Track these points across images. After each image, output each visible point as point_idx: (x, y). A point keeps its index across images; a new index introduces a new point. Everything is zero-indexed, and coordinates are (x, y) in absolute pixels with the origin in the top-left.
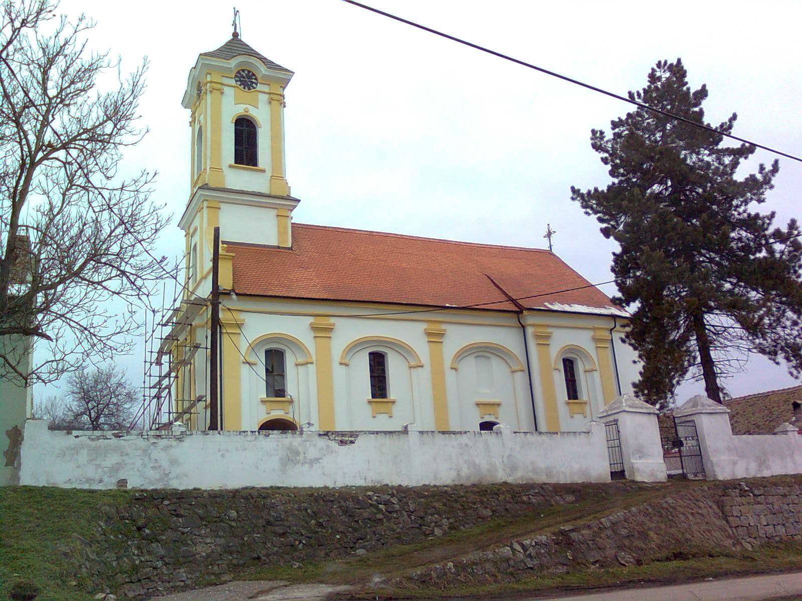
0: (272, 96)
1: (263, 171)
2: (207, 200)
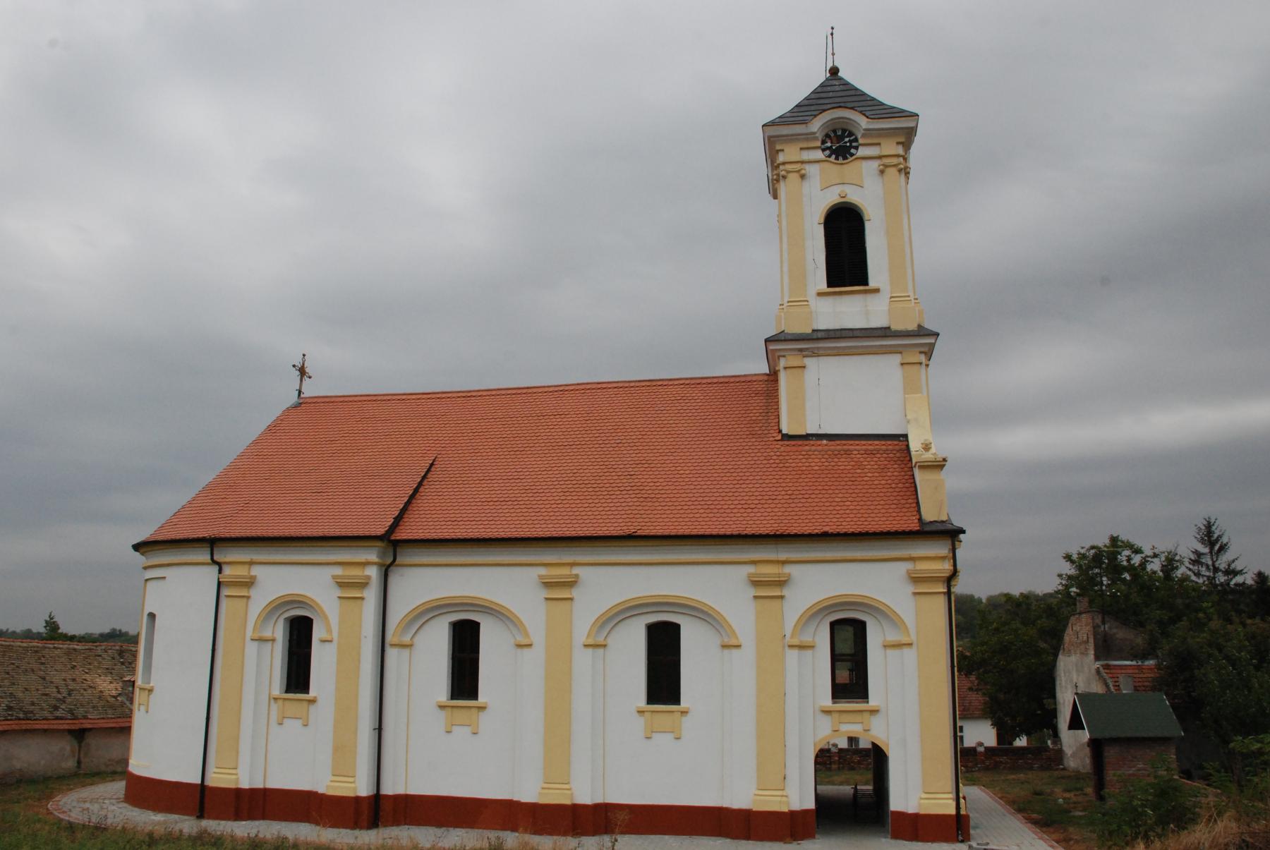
0: (887, 161)
1: (877, 291)
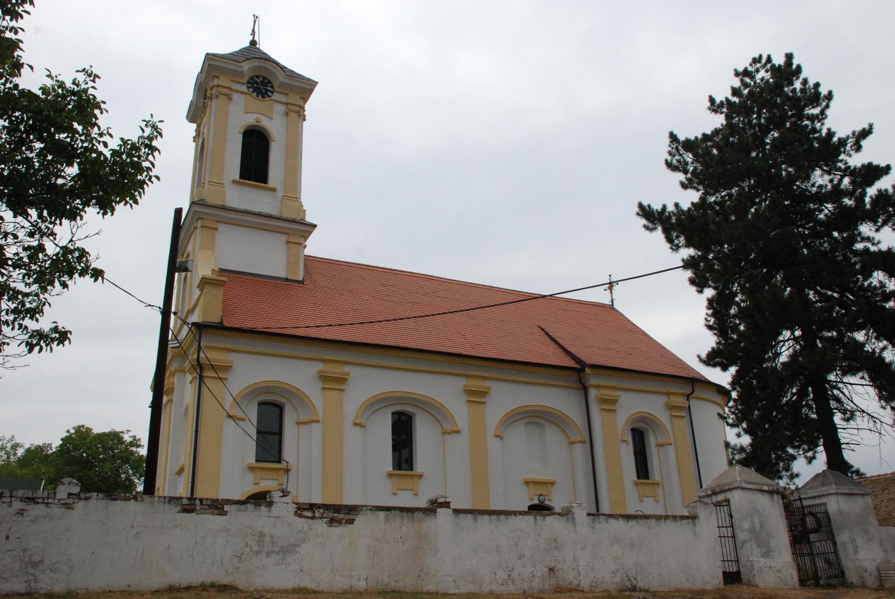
0: (290, 107)
1: (273, 190)
2: (202, 219)
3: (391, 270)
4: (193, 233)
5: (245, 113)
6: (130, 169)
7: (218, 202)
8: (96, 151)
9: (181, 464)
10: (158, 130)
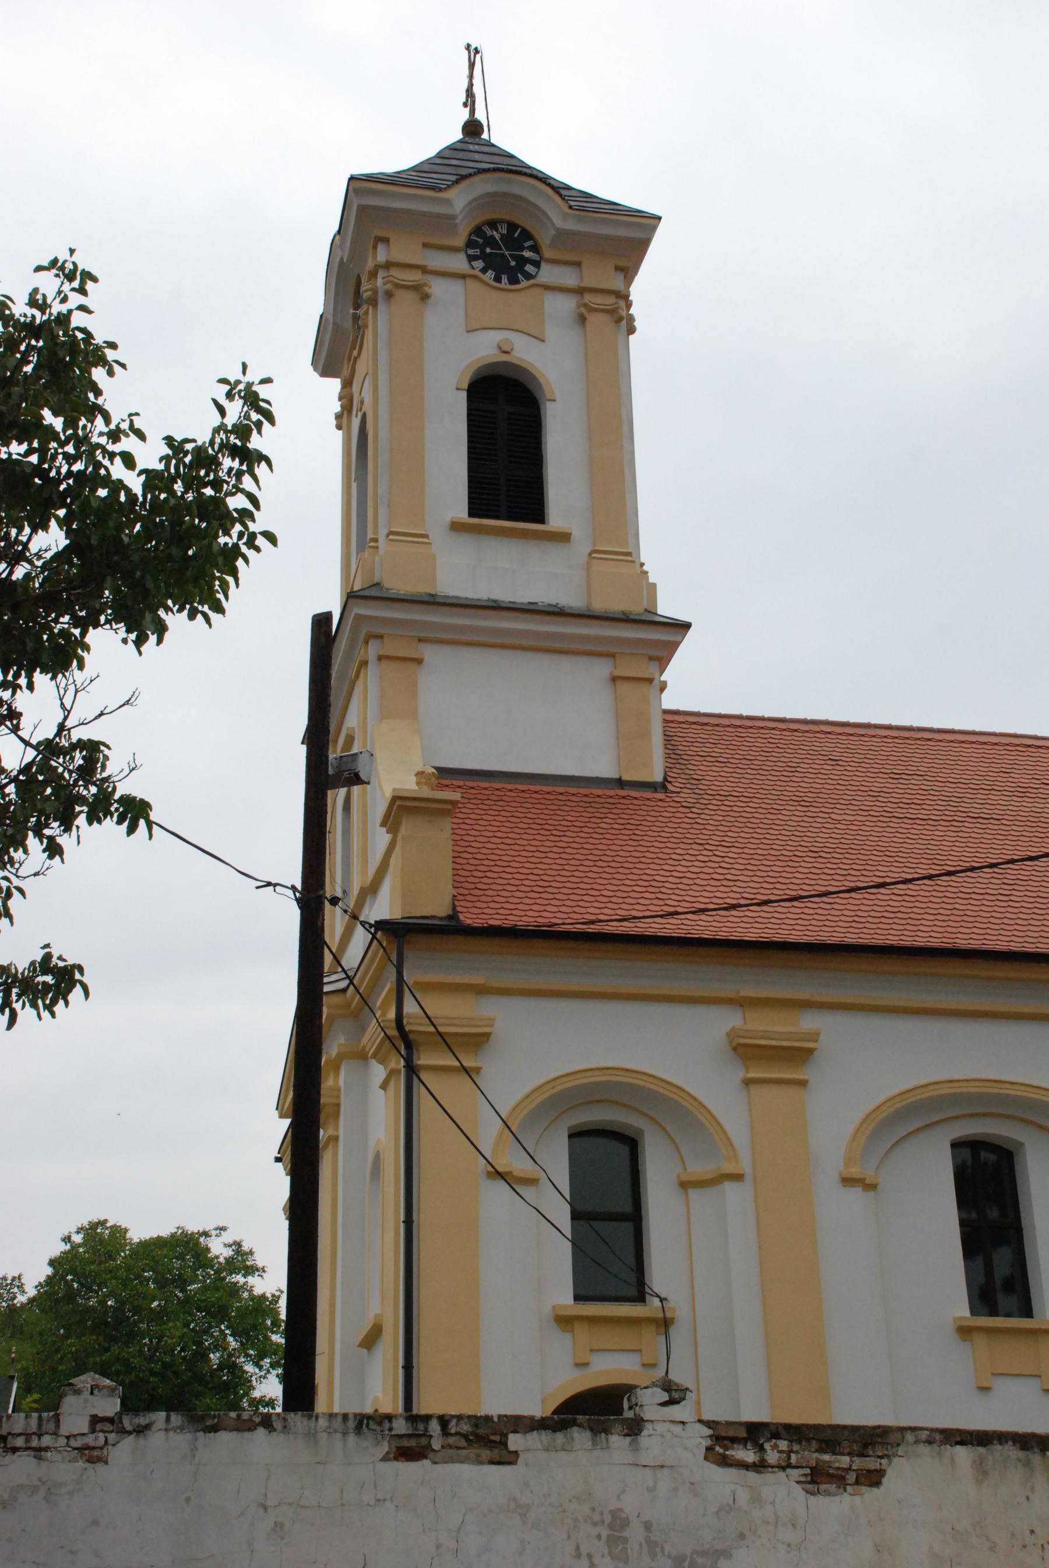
0: (588, 298)
1: (563, 537)
3: (910, 729)
4: (357, 676)
5: (468, 332)
6: (197, 521)
7: (419, 588)
8: (107, 481)
9: (371, 1315)
10: (262, 404)
